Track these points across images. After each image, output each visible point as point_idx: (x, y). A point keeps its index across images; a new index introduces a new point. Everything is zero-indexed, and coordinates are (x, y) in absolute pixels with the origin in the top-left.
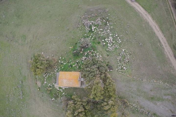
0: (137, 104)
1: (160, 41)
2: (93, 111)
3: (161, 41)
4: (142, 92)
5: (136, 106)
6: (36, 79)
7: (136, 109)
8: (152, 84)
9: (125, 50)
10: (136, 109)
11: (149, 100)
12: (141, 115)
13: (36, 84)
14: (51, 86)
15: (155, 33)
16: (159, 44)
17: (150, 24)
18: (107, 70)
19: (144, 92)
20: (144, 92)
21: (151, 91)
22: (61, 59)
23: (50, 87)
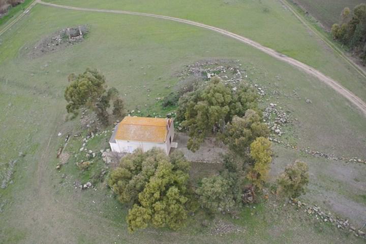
0: (325, 208)
1: (348, 101)
2: (194, 219)
3: (350, 98)
4: (333, 181)
5: (322, 213)
6: (62, 148)
7: (324, 218)
8: (355, 167)
9: (276, 105)
10: (326, 220)
11: (357, 201)
12: (344, 239)
13: (58, 157)
14: (94, 156)
15: (334, 90)
16: (347, 104)
17: (321, 79)
18: (238, 112)
19: (339, 182)
20: (339, 182)
21: (356, 180)
22: (133, 113)
23: (91, 158)
